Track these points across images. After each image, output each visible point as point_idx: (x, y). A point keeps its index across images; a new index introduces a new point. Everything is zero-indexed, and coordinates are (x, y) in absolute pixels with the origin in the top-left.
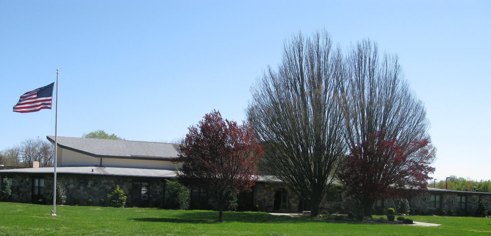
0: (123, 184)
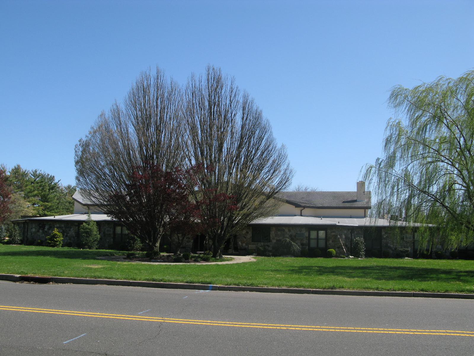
0: (71, 228)
